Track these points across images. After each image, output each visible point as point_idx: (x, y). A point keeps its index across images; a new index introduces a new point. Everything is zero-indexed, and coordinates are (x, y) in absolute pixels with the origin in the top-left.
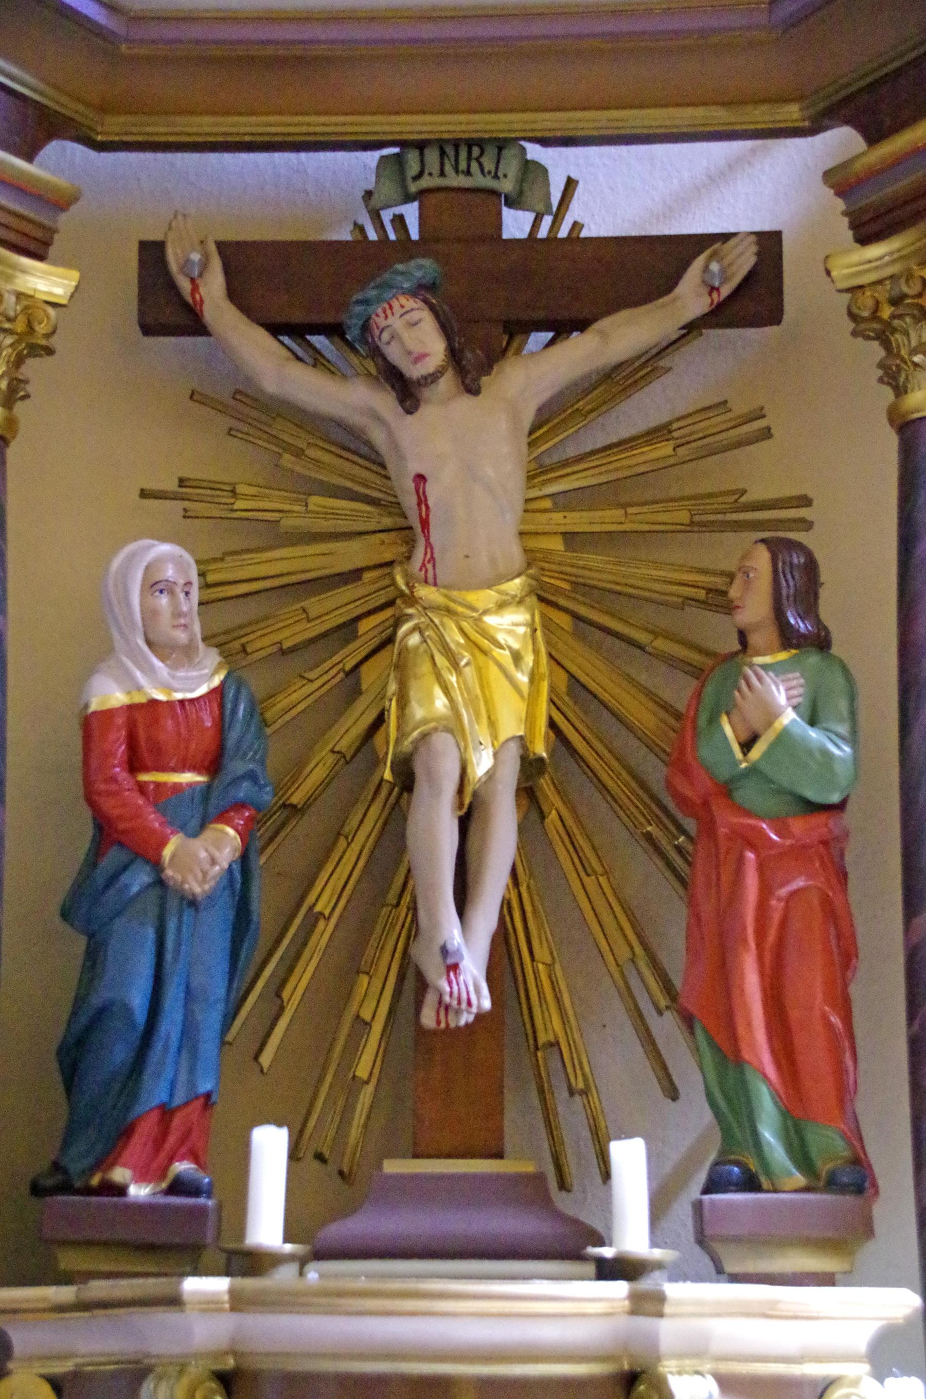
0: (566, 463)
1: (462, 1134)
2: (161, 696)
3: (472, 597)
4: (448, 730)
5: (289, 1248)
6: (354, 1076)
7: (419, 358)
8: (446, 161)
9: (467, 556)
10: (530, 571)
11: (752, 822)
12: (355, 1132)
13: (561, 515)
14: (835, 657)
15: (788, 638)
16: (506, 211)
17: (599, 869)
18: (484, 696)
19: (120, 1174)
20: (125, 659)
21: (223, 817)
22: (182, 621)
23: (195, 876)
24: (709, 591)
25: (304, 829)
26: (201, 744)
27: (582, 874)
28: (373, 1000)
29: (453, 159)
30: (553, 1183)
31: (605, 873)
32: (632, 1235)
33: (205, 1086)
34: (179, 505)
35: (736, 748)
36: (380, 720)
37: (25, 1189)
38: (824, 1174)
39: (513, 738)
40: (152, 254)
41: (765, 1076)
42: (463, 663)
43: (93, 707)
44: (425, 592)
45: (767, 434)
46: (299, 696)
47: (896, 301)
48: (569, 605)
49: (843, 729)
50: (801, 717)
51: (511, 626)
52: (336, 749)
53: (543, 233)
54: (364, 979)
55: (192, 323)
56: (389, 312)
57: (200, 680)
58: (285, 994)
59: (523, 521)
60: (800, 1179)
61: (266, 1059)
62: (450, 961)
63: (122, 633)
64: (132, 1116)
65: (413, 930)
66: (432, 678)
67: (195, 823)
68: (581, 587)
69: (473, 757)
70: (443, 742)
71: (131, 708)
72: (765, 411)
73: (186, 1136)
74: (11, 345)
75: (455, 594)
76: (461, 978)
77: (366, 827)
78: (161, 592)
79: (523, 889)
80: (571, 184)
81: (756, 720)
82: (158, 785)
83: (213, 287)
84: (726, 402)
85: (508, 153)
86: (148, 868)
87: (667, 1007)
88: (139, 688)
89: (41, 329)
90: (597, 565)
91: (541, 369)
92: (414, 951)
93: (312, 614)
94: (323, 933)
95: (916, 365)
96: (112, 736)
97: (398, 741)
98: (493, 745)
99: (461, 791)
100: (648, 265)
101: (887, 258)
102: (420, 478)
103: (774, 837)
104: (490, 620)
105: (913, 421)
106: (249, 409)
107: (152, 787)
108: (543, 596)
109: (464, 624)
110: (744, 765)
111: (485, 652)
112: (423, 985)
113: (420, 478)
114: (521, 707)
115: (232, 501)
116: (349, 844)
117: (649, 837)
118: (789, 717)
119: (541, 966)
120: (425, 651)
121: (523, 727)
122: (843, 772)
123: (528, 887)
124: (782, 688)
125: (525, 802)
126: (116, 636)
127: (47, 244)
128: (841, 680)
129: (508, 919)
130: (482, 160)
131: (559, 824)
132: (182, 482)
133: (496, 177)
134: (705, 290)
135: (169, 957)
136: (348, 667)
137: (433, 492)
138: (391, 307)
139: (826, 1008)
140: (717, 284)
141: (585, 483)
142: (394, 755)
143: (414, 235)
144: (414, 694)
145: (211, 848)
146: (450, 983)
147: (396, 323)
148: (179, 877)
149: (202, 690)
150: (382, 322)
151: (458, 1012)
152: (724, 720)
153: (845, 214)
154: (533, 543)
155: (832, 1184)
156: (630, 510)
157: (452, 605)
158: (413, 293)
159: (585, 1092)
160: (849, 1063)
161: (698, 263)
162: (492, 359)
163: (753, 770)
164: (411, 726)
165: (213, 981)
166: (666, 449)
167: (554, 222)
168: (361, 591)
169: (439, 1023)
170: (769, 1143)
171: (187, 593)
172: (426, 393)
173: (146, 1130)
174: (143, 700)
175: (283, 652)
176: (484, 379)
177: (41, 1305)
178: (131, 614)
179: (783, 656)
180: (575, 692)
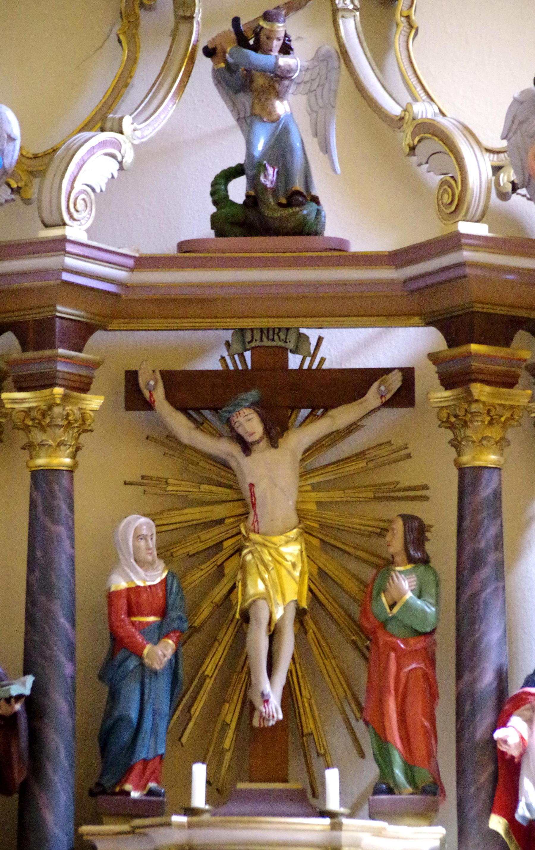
0: (317, 469)
1: (271, 766)
2: (140, 583)
3: (275, 539)
4: (265, 599)
5: (207, 807)
6: (223, 748)
7: (251, 435)
8: (263, 335)
9: (272, 520)
10: (300, 526)
11: (394, 640)
12: (223, 771)
13: (316, 493)
14: (431, 567)
15: (411, 560)
16: (290, 355)
17: (331, 656)
18: (280, 582)
19: (128, 787)
20: (126, 568)
21: (167, 636)
22: (150, 552)
23: (157, 663)
24: (382, 529)
25: (198, 638)
26: (158, 602)
27: (324, 658)
28: (230, 714)
29: (266, 334)
30: (309, 794)
31: (334, 658)
32: (333, 803)
33: (161, 751)
34: (141, 488)
35: (387, 608)
36: (234, 587)
37: (86, 793)
38: (421, 788)
39: (293, 601)
40: (132, 377)
41: (396, 747)
42: (270, 569)
43: (113, 589)
44: (254, 536)
45: (409, 456)
46: (198, 576)
47: (456, 416)
48: (321, 536)
49: (432, 601)
50: (414, 594)
51: (292, 551)
52: (214, 601)
53: (306, 367)
54: (227, 705)
55: (149, 406)
56: (238, 415)
57: (156, 576)
58: (192, 711)
59: (299, 497)
60: (410, 789)
61: (184, 740)
62: (266, 698)
63: (123, 555)
64: (132, 763)
65: (249, 685)
66: (257, 575)
67: (156, 639)
68: (322, 526)
69: (275, 610)
70: (262, 604)
71: (128, 590)
72: (408, 446)
73: (153, 772)
74: (77, 432)
75: (267, 538)
76: (270, 706)
77: (227, 636)
78: (141, 539)
79: (298, 665)
80: (320, 339)
81: (395, 596)
82: (140, 622)
83: (159, 396)
84: (390, 442)
85: (291, 332)
86: (137, 659)
87: (361, 718)
88: (132, 581)
89: (88, 422)
90: (331, 516)
91: (301, 437)
92: (249, 695)
93: (203, 538)
94: (209, 684)
95: (464, 445)
96: (121, 602)
97: (242, 604)
98: (284, 604)
99: (270, 624)
100: (353, 383)
101: (452, 397)
102: (252, 485)
103: (402, 646)
104: (283, 549)
105: (464, 468)
106: (171, 443)
107: (137, 623)
108: (307, 531)
109: (272, 551)
110: (390, 615)
111: (280, 563)
112: (253, 709)
113: (252, 485)
114: (295, 587)
115: (166, 486)
116: (220, 644)
117: (353, 641)
118: (409, 595)
119: (305, 700)
120: (254, 562)
121: (296, 596)
122: (432, 619)
123: (300, 664)
124: (407, 582)
125: (298, 625)
126: (121, 557)
127: (90, 383)
128: (432, 578)
129: (290, 677)
130: (280, 334)
131: (313, 635)
132: (143, 477)
133: (286, 342)
134: (378, 396)
135: (146, 697)
136: (219, 563)
137: (258, 492)
138: (240, 414)
139: (423, 719)
140: (384, 394)
141: (328, 478)
142: (241, 610)
143: (250, 368)
144: (249, 582)
145: (164, 651)
146: (265, 708)
147: (241, 419)
148: (150, 663)
149: (158, 580)
150: (235, 419)
151: (269, 720)
152: (383, 596)
153: (437, 372)
154: (302, 506)
155: (424, 791)
156: (346, 491)
157: (266, 543)
158: (249, 407)
159: (324, 755)
160: (433, 742)
161: (376, 385)
162: (281, 435)
163: (394, 617)
164: (248, 597)
165: (164, 706)
166: (362, 464)
167: (311, 360)
168: (224, 529)
169: (260, 724)
170: (398, 775)
171: (152, 539)
172: (255, 448)
173: (137, 769)
174: (134, 586)
175: (190, 556)
176: (280, 440)
177: (110, 833)
178: (128, 548)
179: (409, 567)
180: (322, 575)
